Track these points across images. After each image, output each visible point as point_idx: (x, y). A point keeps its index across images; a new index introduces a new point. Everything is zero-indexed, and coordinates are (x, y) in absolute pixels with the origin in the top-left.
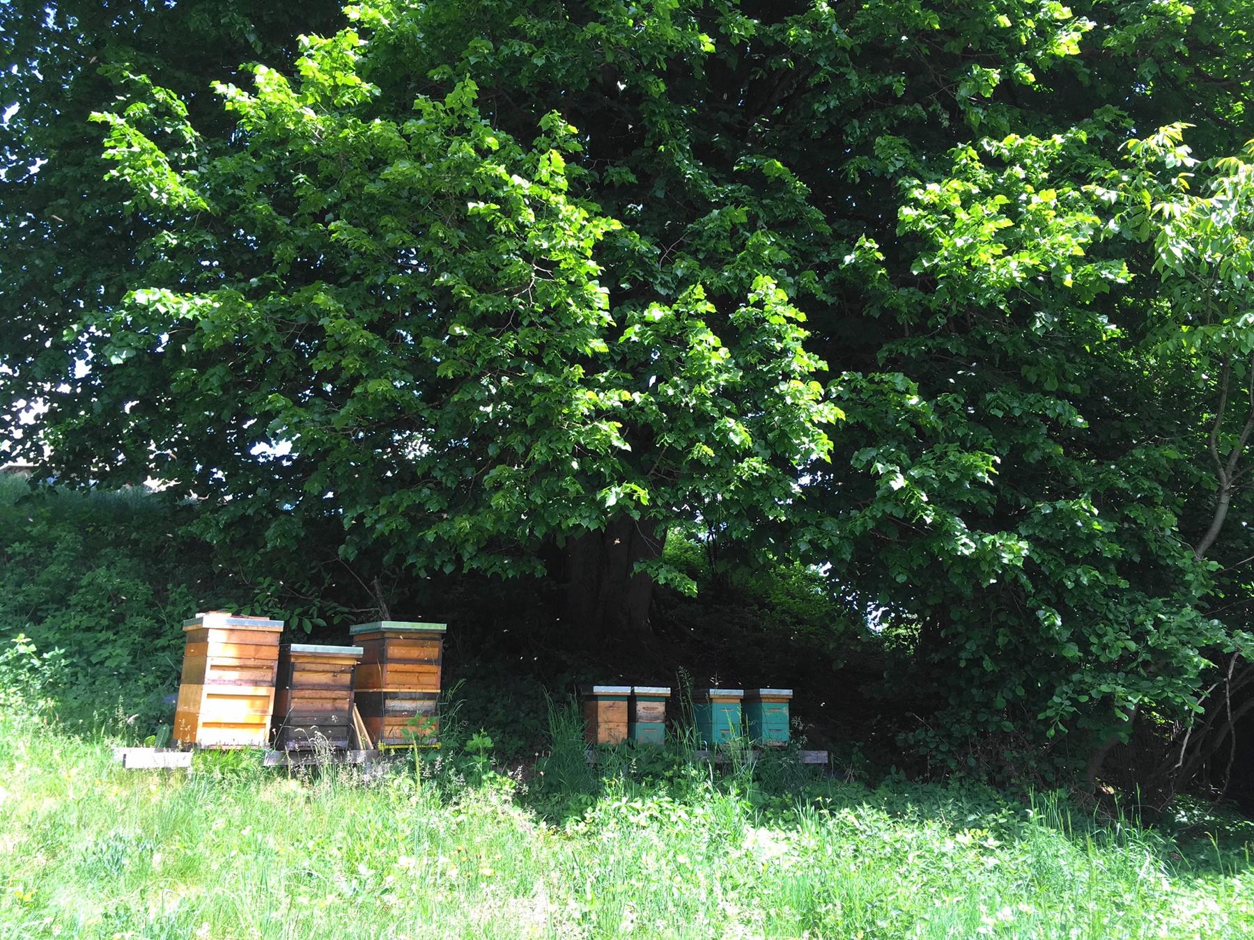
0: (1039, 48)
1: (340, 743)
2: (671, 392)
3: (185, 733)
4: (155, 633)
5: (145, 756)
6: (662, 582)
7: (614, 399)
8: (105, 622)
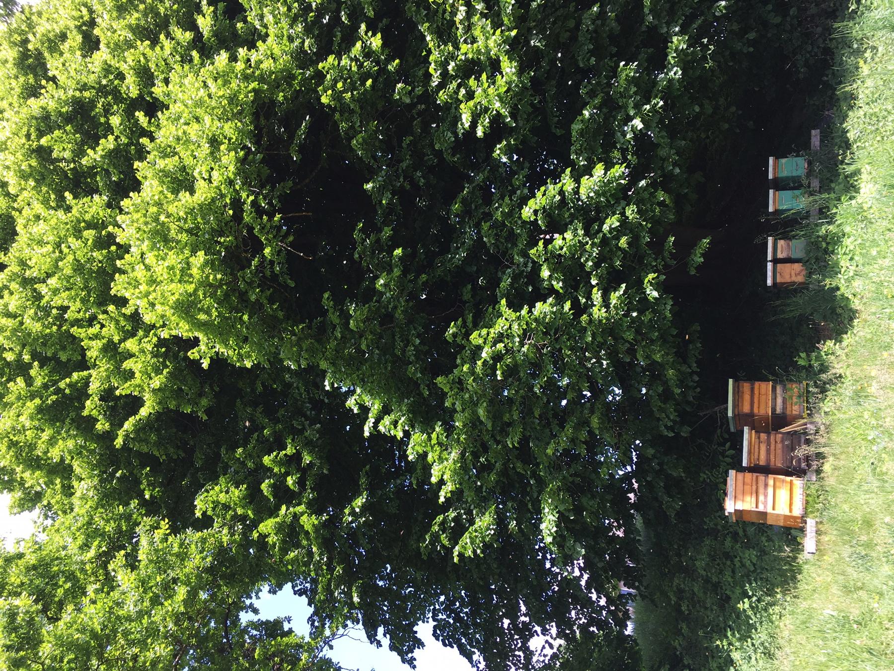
0: (379, 57)
1: (803, 440)
2: (590, 263)
3: (795, 522)
4: (735, 536)
5: (809, 543)
6: (702, 260)
7: (597, 295)
8: (729, 563)
